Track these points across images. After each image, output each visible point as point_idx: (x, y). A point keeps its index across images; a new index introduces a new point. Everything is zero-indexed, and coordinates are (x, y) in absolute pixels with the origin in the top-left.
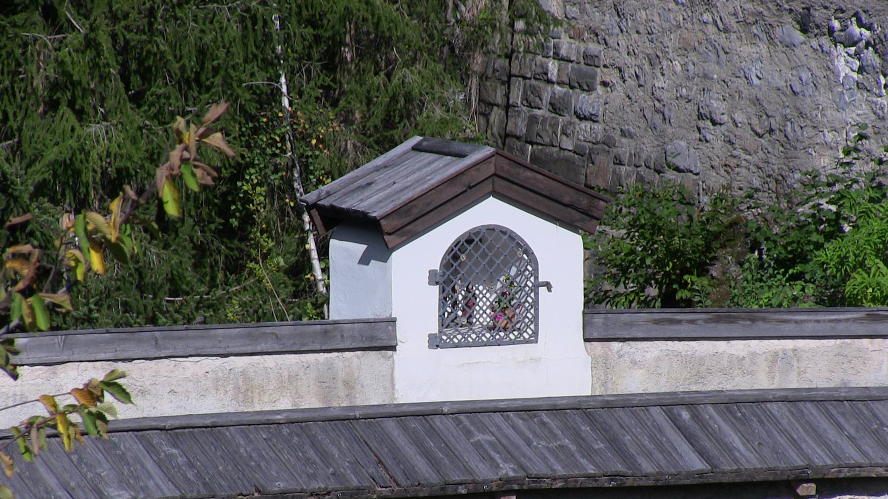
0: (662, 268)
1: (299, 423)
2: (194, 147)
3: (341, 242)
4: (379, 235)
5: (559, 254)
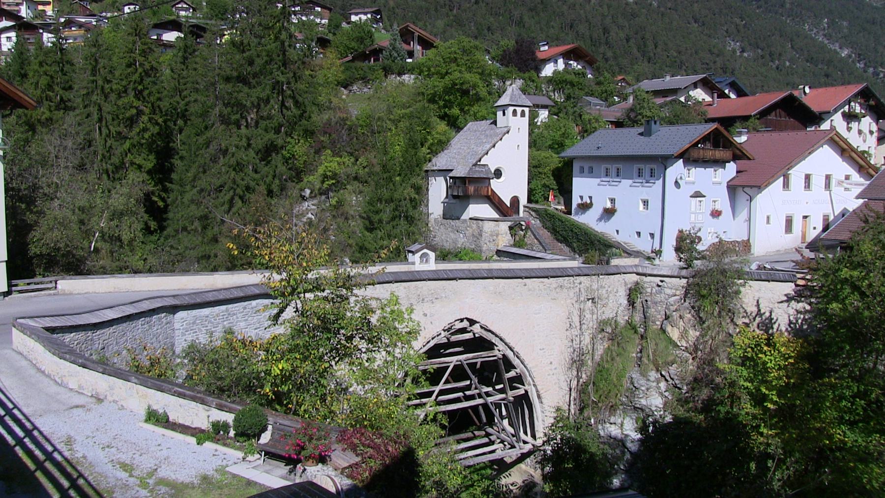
0: (443, 256)
1: (405, 272)
2: (394, 243)
3: (49, 355)
4: (413, 253)
5: (432, 255)
